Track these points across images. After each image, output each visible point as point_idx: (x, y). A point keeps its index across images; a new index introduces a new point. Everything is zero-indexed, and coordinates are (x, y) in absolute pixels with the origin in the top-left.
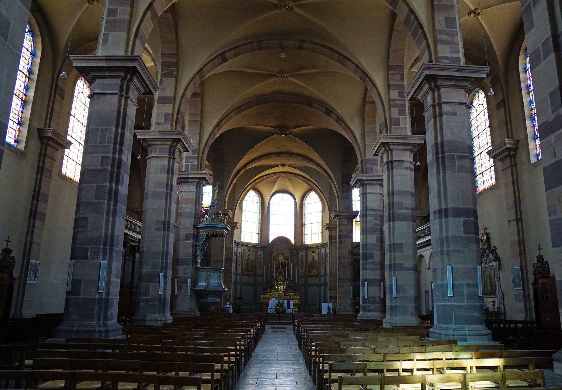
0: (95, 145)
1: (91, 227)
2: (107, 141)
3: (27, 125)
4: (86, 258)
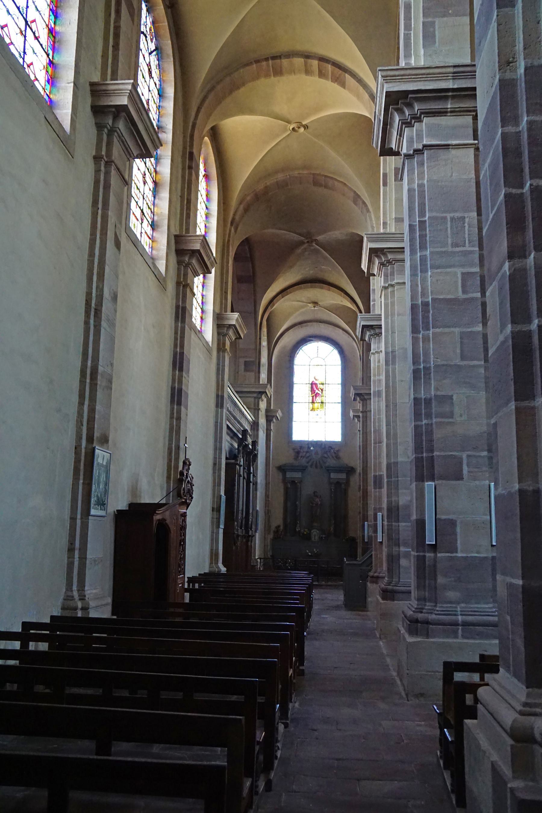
0: (443, 249)
1: (461, 416)
2: (467, 241)
3: (166, 228)
4: (459, 477)
